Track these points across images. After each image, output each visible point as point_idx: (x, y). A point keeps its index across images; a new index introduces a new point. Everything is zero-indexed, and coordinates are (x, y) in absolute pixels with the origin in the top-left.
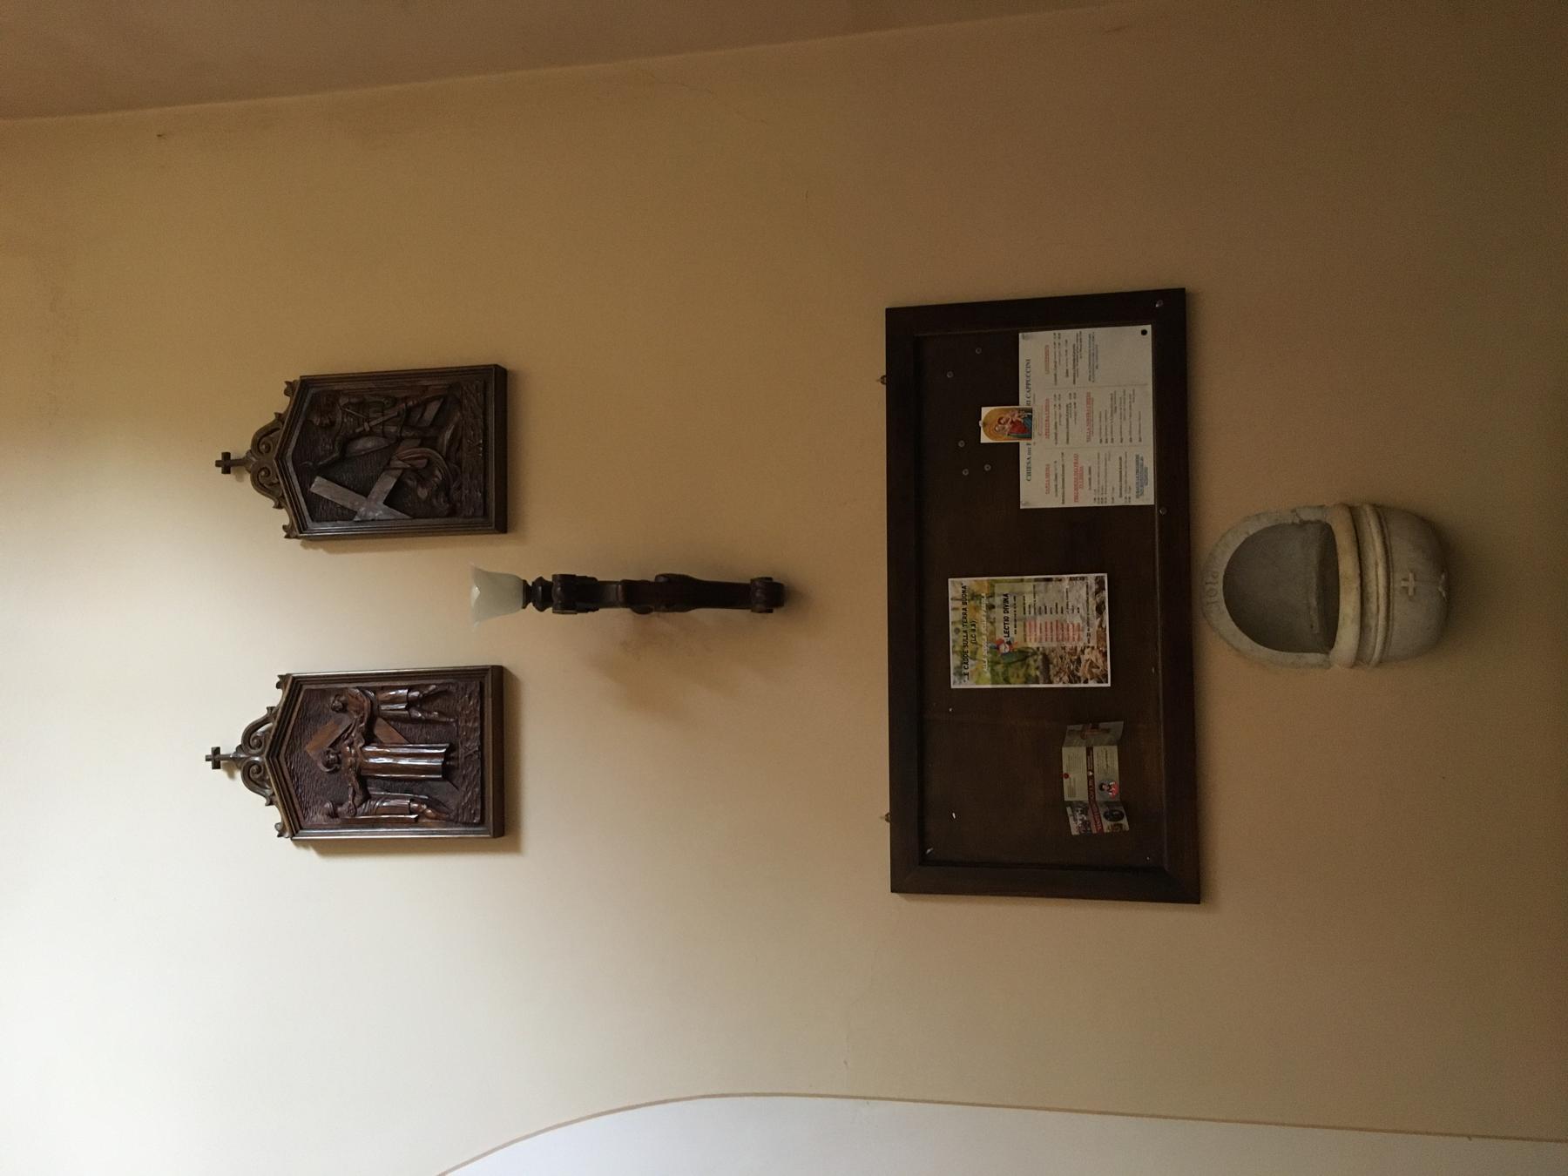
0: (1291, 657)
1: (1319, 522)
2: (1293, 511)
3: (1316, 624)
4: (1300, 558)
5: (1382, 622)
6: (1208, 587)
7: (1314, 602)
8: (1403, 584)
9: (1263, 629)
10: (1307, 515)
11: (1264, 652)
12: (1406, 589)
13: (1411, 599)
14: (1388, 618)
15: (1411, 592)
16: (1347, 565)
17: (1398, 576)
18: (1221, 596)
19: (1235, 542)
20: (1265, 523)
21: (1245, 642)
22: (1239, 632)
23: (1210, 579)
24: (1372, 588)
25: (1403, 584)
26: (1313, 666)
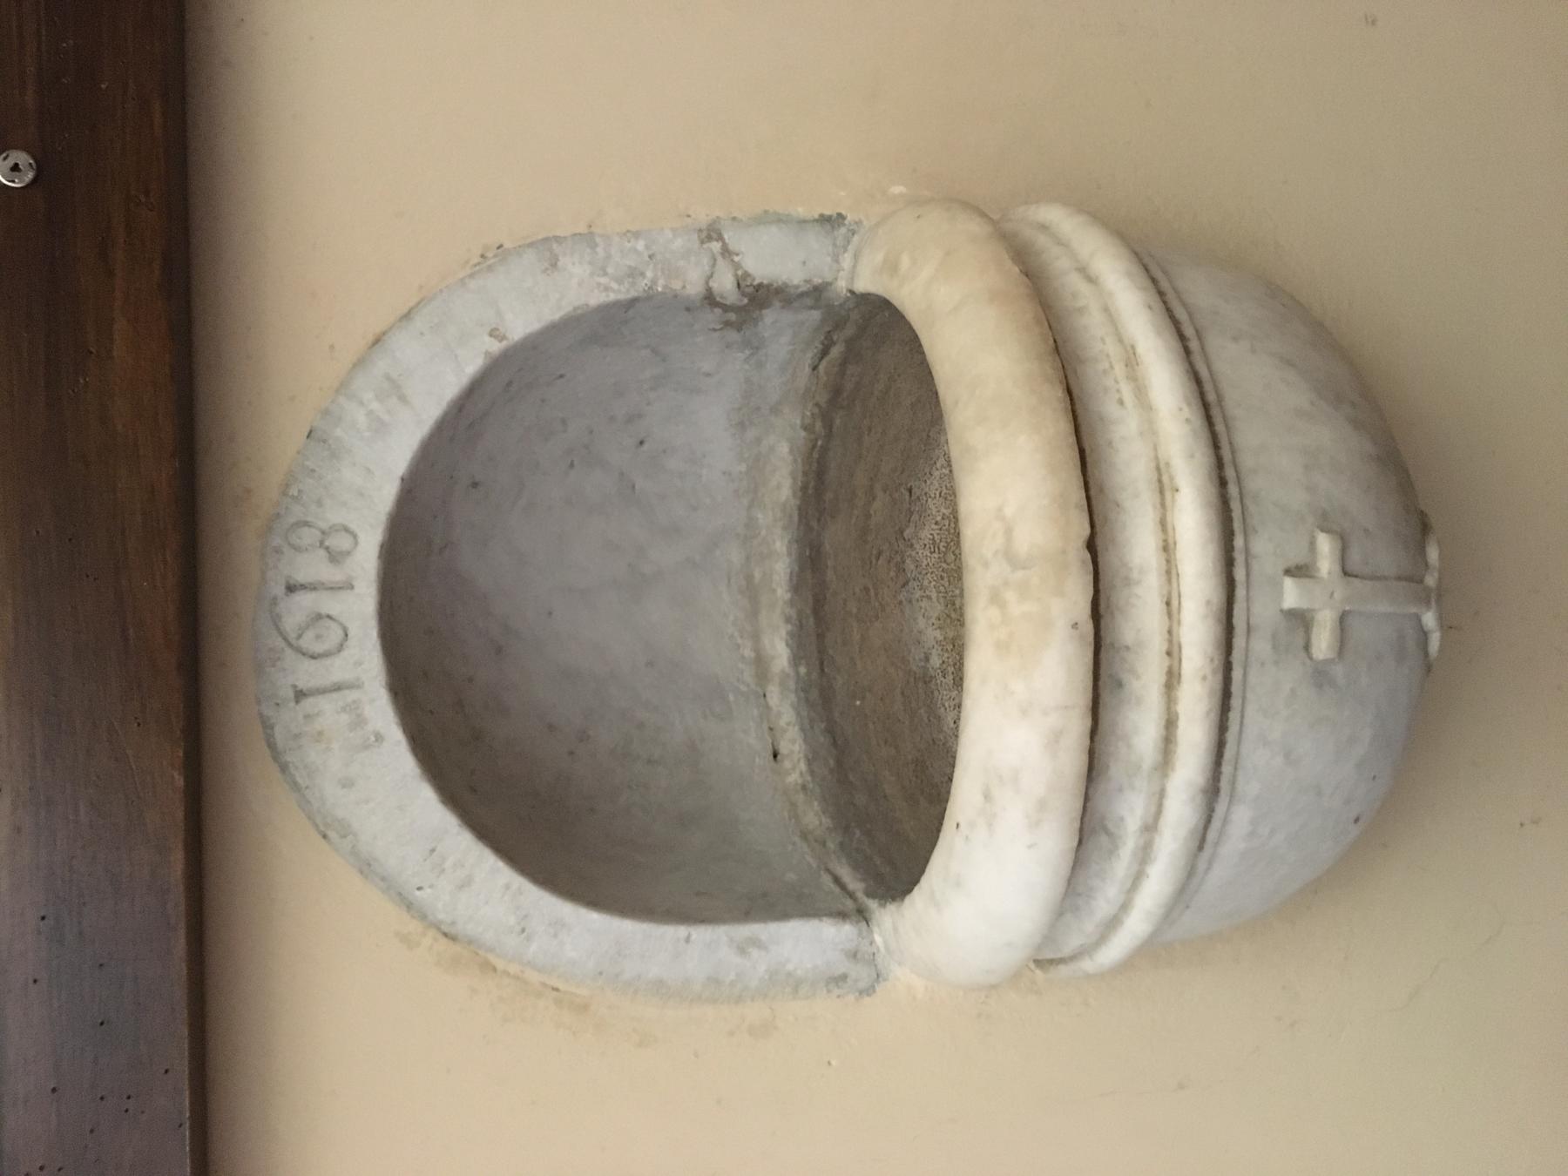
0: (700, 949)
1: (817, 293)
2: (712, 233)
3: (793, 745)
4: (731, 451)
5: (1180, 809)
6: (306, 674)
7: (779, 651)
8: (1292, 595)
9: (541, 793)
10: (775, 258)
11: (579, 933)
12: (1301, 620)
13: (1320, 676)
14: (1213, 790)
15: (1323, 642)
16: (1004, 487)
17: (1266, 548)
18: (360, 608)
19: (434, 376)
20: (579, 287)
21: (487, 891)
22: (461, 843)
23: (312, 567)
24: (1141, 619)
25: (1292, 595)
26: (795, 985)
